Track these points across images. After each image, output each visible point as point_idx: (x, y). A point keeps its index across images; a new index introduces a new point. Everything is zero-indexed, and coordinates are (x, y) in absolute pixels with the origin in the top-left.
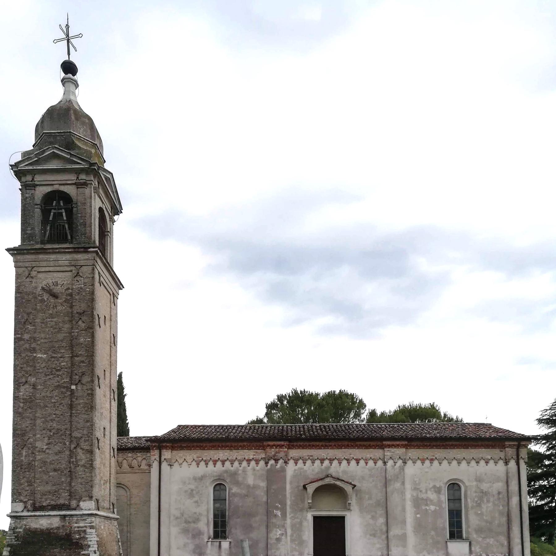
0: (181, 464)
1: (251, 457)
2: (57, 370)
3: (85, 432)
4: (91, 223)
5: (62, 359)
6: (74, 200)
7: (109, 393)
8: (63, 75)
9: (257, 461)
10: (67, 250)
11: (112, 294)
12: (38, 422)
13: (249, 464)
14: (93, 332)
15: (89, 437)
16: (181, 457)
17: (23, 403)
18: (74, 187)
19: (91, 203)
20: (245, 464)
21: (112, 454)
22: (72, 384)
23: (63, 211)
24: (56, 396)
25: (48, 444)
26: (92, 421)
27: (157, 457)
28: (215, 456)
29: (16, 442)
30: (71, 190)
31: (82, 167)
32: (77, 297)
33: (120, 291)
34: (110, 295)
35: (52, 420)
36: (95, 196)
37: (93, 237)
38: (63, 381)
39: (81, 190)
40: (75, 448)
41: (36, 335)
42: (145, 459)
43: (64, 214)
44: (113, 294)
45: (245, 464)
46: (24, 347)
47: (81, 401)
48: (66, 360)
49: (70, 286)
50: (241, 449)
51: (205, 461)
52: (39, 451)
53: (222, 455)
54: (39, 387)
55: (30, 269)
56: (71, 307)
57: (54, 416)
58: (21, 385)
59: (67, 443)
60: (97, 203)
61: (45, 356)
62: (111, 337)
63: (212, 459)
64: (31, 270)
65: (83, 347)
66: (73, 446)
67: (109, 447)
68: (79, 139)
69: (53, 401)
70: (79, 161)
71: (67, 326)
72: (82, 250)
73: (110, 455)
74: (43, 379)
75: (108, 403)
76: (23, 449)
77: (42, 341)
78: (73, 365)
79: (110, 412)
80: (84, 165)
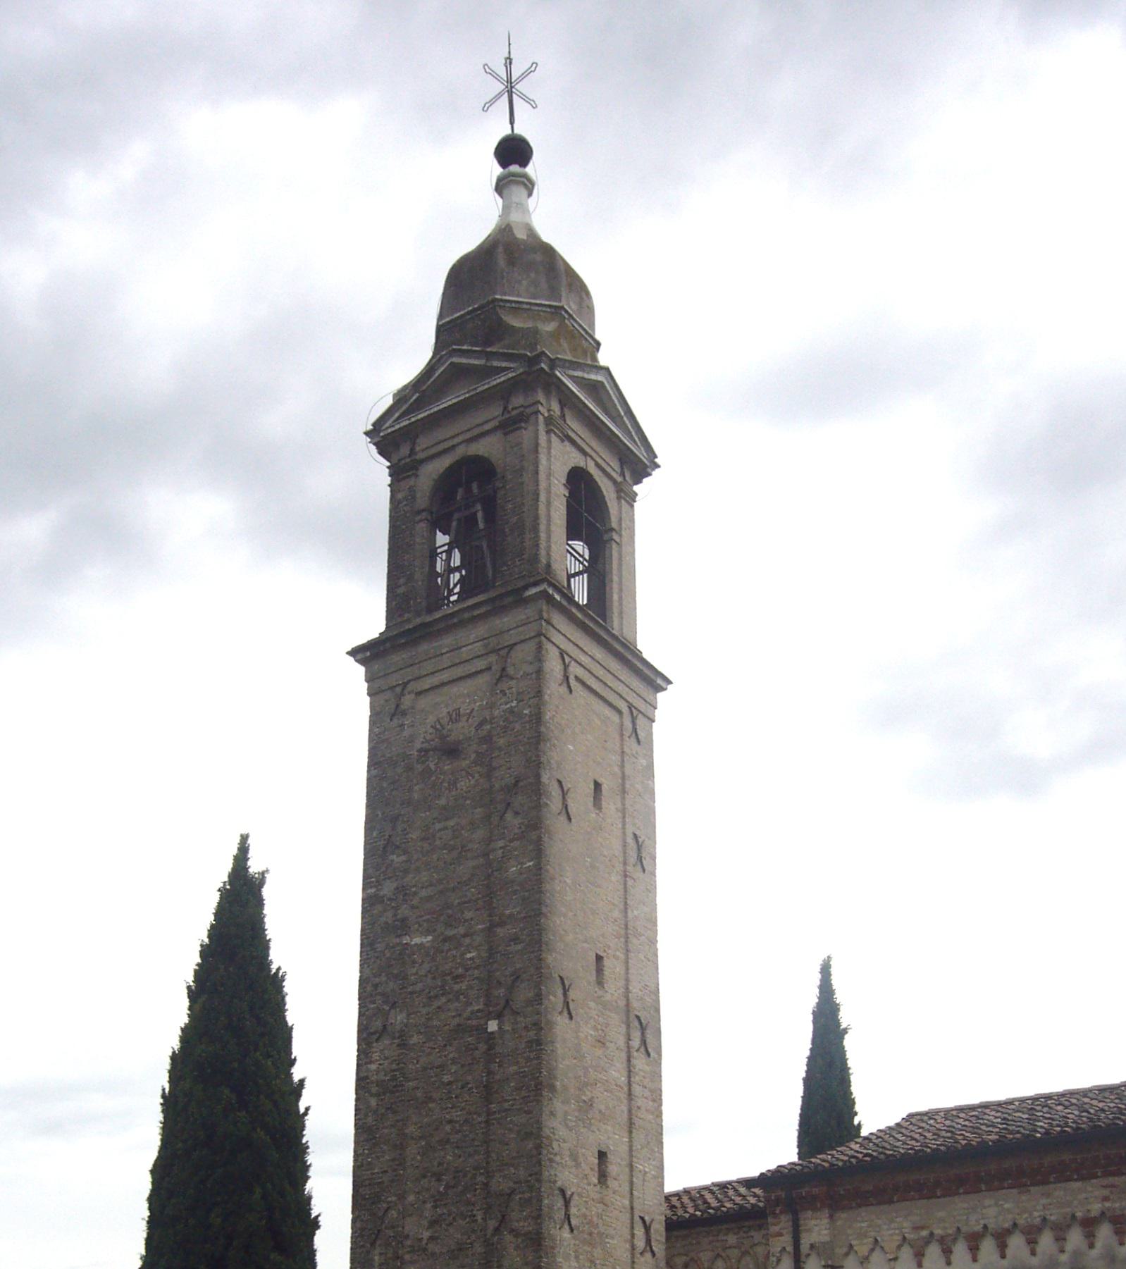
0: (865, 1260)
1: (1096, 1208)
2: (458, 978)
3: (522, 1174)
4: (537, 517)
5: (467, 941)
6: (498, 470)
7: (623, 1029)
8: (498, 170)
9: (1089, 1225)
10: (476, 613)
11: (625, 710)
12: (412, 1150)
13: (1090, 1238)
14: (540, 839)
15: (531, 1188)
16: (862, 1235)
17: (378, 1095)
18: (499, 434)
19: (536, 464)
20: (1075, 1238)
21: (640, 1243)
22: (489, 1016)
23: (479, 507)
24: (454, 1061)
25: (433, 1223)
26: (539, 1136)
27: (786, 1240)
28: (973, 1218)
29: (358, 1225)
30: (489, 448)
31: (510, 375)
32: (501, 742)
33: (660, 695)
34: (620, 712)
35: (444, 1142)
36: (549, 441)
37: (543, 552)
38: (469, 1009)
39: (511, 438)
40: (497, 1230)
41: (409, 879)
42: (718, 1256)
43: (480, 515)
44: (630, 707)
45: (1075, 1238)
46: (383, 919)
47: (514, 1069)
48: (478, 939)
49: (487, 714)
50: (1058, 1181)
51: (942, 1240)
52: (413, 1250)
53: (992, 1212)
54: (415, 1040)
55: (398, 690)
56: (489, 775)
57: (448, 1128)
58: (375, 1037)
59: (479, 1218)
60: (556, 462)
61: (430, 938)
62: (625, 845)
63: (964, 1229)
64: (402, 694)
65: (515, 892)
66: (492, 1224)
67: (626, 1217)
68: (517, 309)
69: (446, 1078)
70: (504, 364)
71: (480, 834)
72: (510, 599)
73: (633, 1248)
74: (424, 1011)
75: (620, 1064)
76: (373, 1244)
77: (424, 893)
78: (492, 952)
79: (630, 1094)
80: (515, 370)
